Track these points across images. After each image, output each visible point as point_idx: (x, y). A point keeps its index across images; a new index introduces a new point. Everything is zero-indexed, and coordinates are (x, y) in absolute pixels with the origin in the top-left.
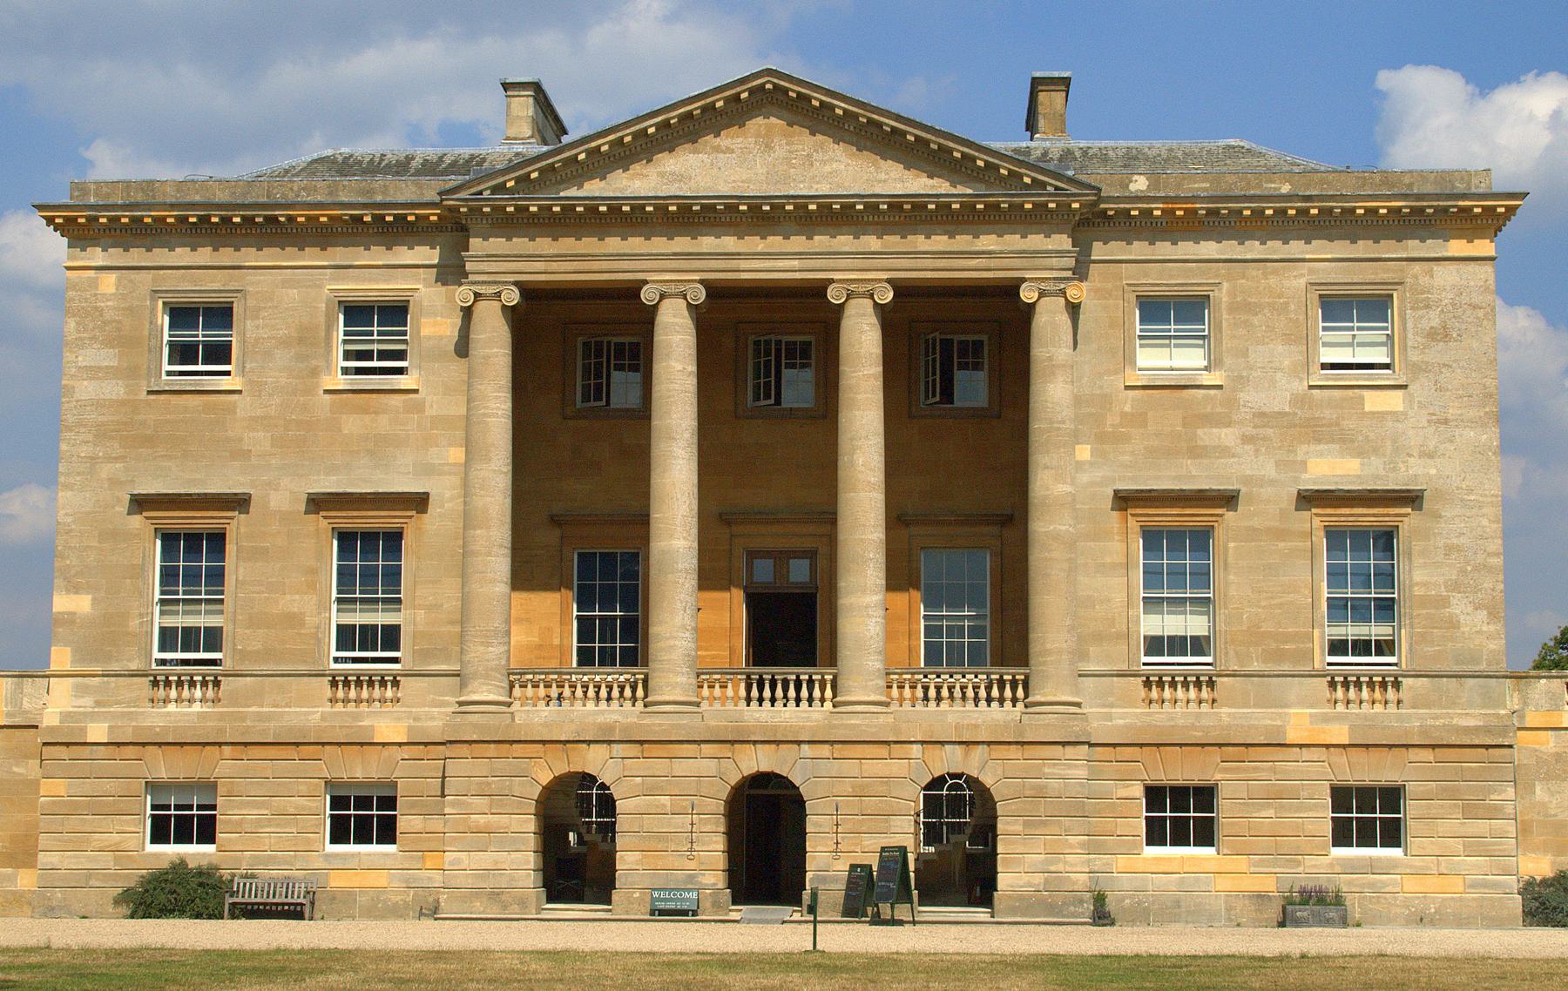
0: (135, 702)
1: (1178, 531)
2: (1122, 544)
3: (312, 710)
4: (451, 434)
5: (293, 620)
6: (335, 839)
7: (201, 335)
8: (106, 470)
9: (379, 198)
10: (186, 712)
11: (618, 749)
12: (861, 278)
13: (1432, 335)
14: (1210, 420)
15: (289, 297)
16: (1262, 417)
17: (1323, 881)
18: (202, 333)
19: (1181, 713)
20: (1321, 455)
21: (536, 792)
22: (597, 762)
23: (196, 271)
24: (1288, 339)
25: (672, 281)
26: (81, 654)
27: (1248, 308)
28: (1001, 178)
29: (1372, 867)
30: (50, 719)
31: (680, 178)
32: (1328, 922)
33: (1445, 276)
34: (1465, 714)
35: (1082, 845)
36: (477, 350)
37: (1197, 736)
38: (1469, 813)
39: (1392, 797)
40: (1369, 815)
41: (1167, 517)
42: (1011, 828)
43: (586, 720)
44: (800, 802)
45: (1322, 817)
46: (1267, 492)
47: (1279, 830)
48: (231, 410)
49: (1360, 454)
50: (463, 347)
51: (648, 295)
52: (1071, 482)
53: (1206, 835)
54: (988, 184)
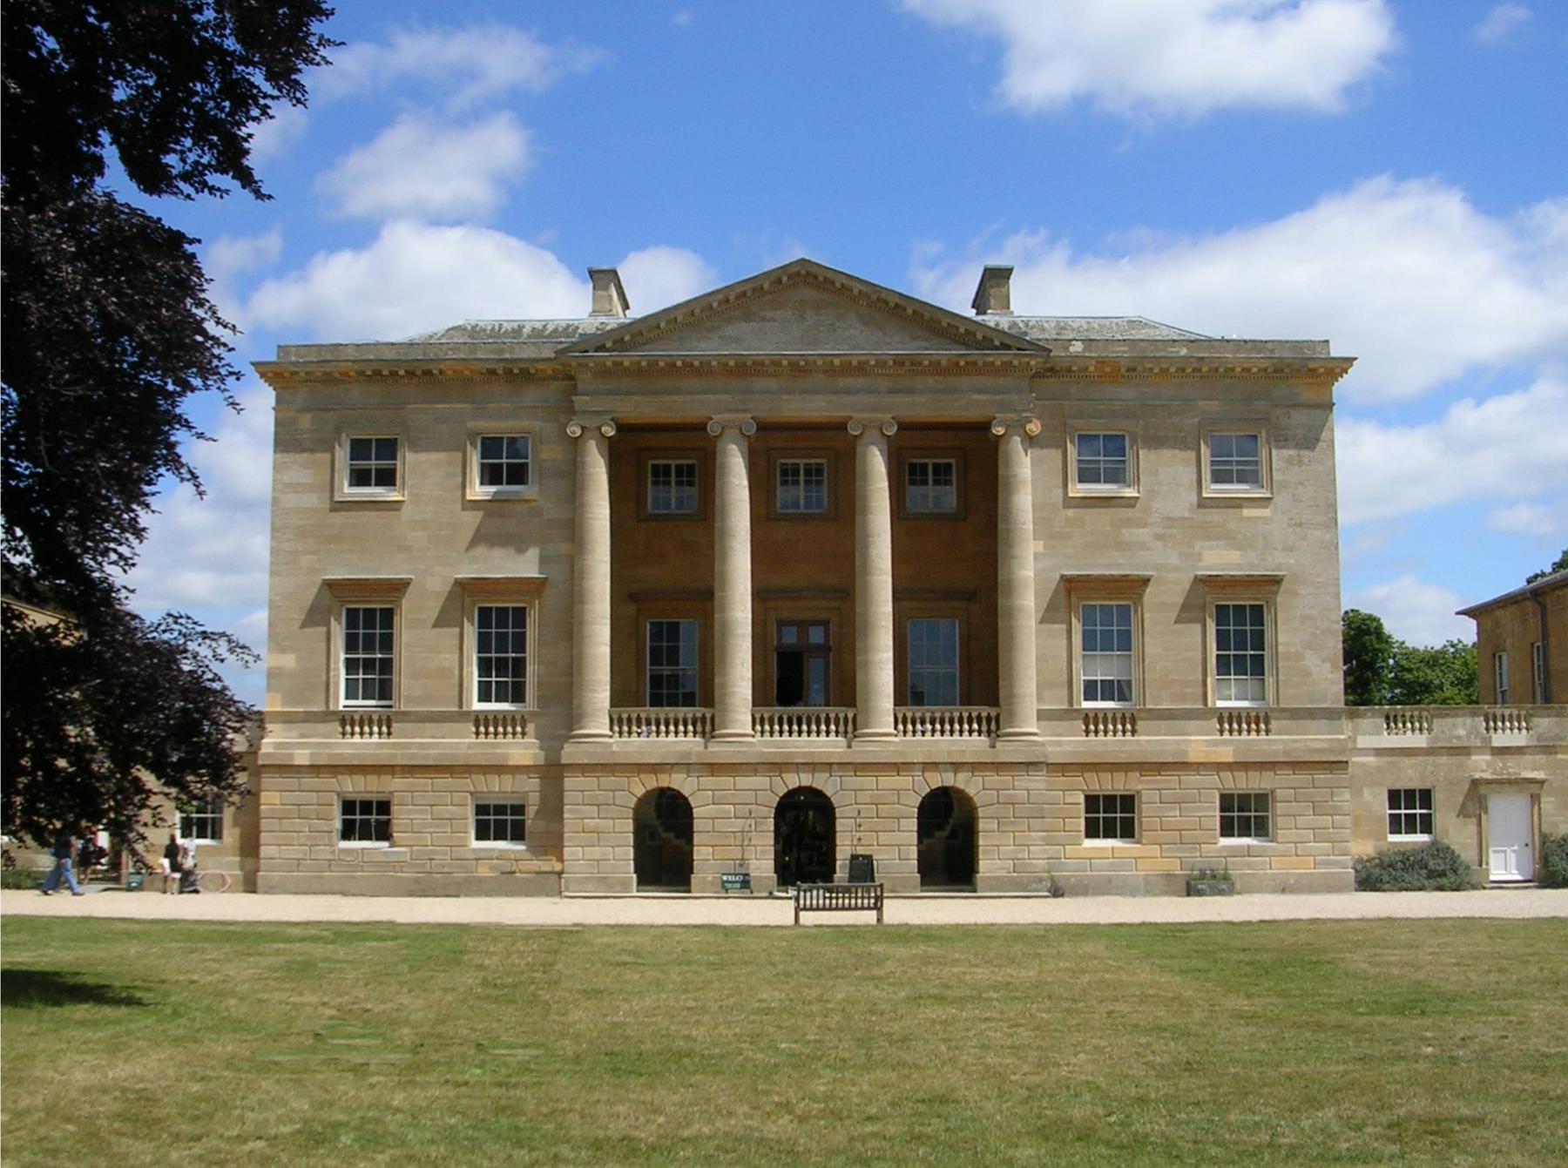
1: (1103, 609)
3: (461, 743)
6: (479, 837)
7: (373, 464)
8: (305, 561)
9: (508, 356)
12: (873, 414)
14: (1130, 523)
16: (1170, 521)
17: (1219, 865)
19: (1112, 744)
20: (1212, 548)
21: (633, 802)
28: (978, 342)
29: (1249, 852)
32: (1221, 893)
34: (1314, 739)
35: (1043, 838)
37: (1123, 758)
40: (1244, 815)
42: (988, 827)
45: (1215, 816)
46: (1172, 576)
53: (1128, 831)
54: (968, 347)
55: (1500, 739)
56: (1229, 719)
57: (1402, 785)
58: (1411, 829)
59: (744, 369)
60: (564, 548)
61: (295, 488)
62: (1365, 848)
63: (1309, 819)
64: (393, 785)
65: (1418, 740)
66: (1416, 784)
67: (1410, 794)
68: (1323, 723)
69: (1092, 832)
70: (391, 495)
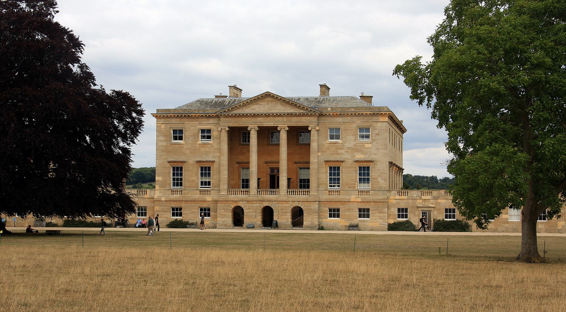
0: (169, 194)
2: (325, 176)
3: (196, 195)
4: (218, 151)
5: (193, 181)
8: (163, 157)
10: (176, 196)
11: (244, 202)
12: (283, 125)
13: (376, 134)
15: (192, 128)
18: (178, 135)
19: (334, 197)
22: (241, 204)
23: (177, 124)
24: (353, 135)
25: (253, 126)
26: (160, 187)
27: (347, 130)
29: (364, 221)
30: (156, 197)
31: (254, 109)
33: (379, 124)
36: (222, 138)
37: (337, 200)
38: (380, 212)
39: (368, 210)
41: (333, 165)
43: (238, 198)
44: (273, 211)
45: (357, 213)
47: (350, 215)
48: (183, 147)
49: (364, 154)
50: (220, 138)
51: (249, 129)
52: (317, 159)
53: (338, 216)
55: (423, 197)
56: (361, 192)
57: (401, 207)
58: (403, 217)
59: (255, 116)
60: (219, 154)
61: (161, 141)
62: (392, 221)
63: (377, 214)
64: (183, 205)
65: (405, 197)
66: (404, 207)
67: (403, 209)
68: (84, 233)
69: (330, 216)
70: (339, 141)
